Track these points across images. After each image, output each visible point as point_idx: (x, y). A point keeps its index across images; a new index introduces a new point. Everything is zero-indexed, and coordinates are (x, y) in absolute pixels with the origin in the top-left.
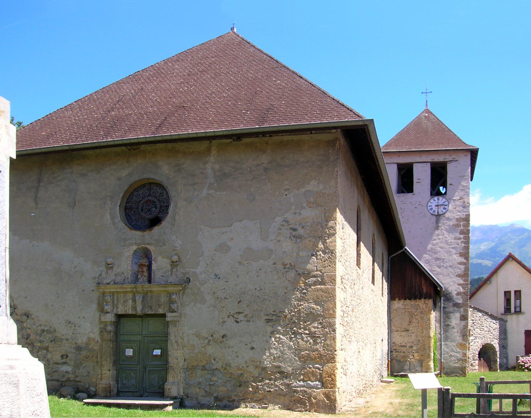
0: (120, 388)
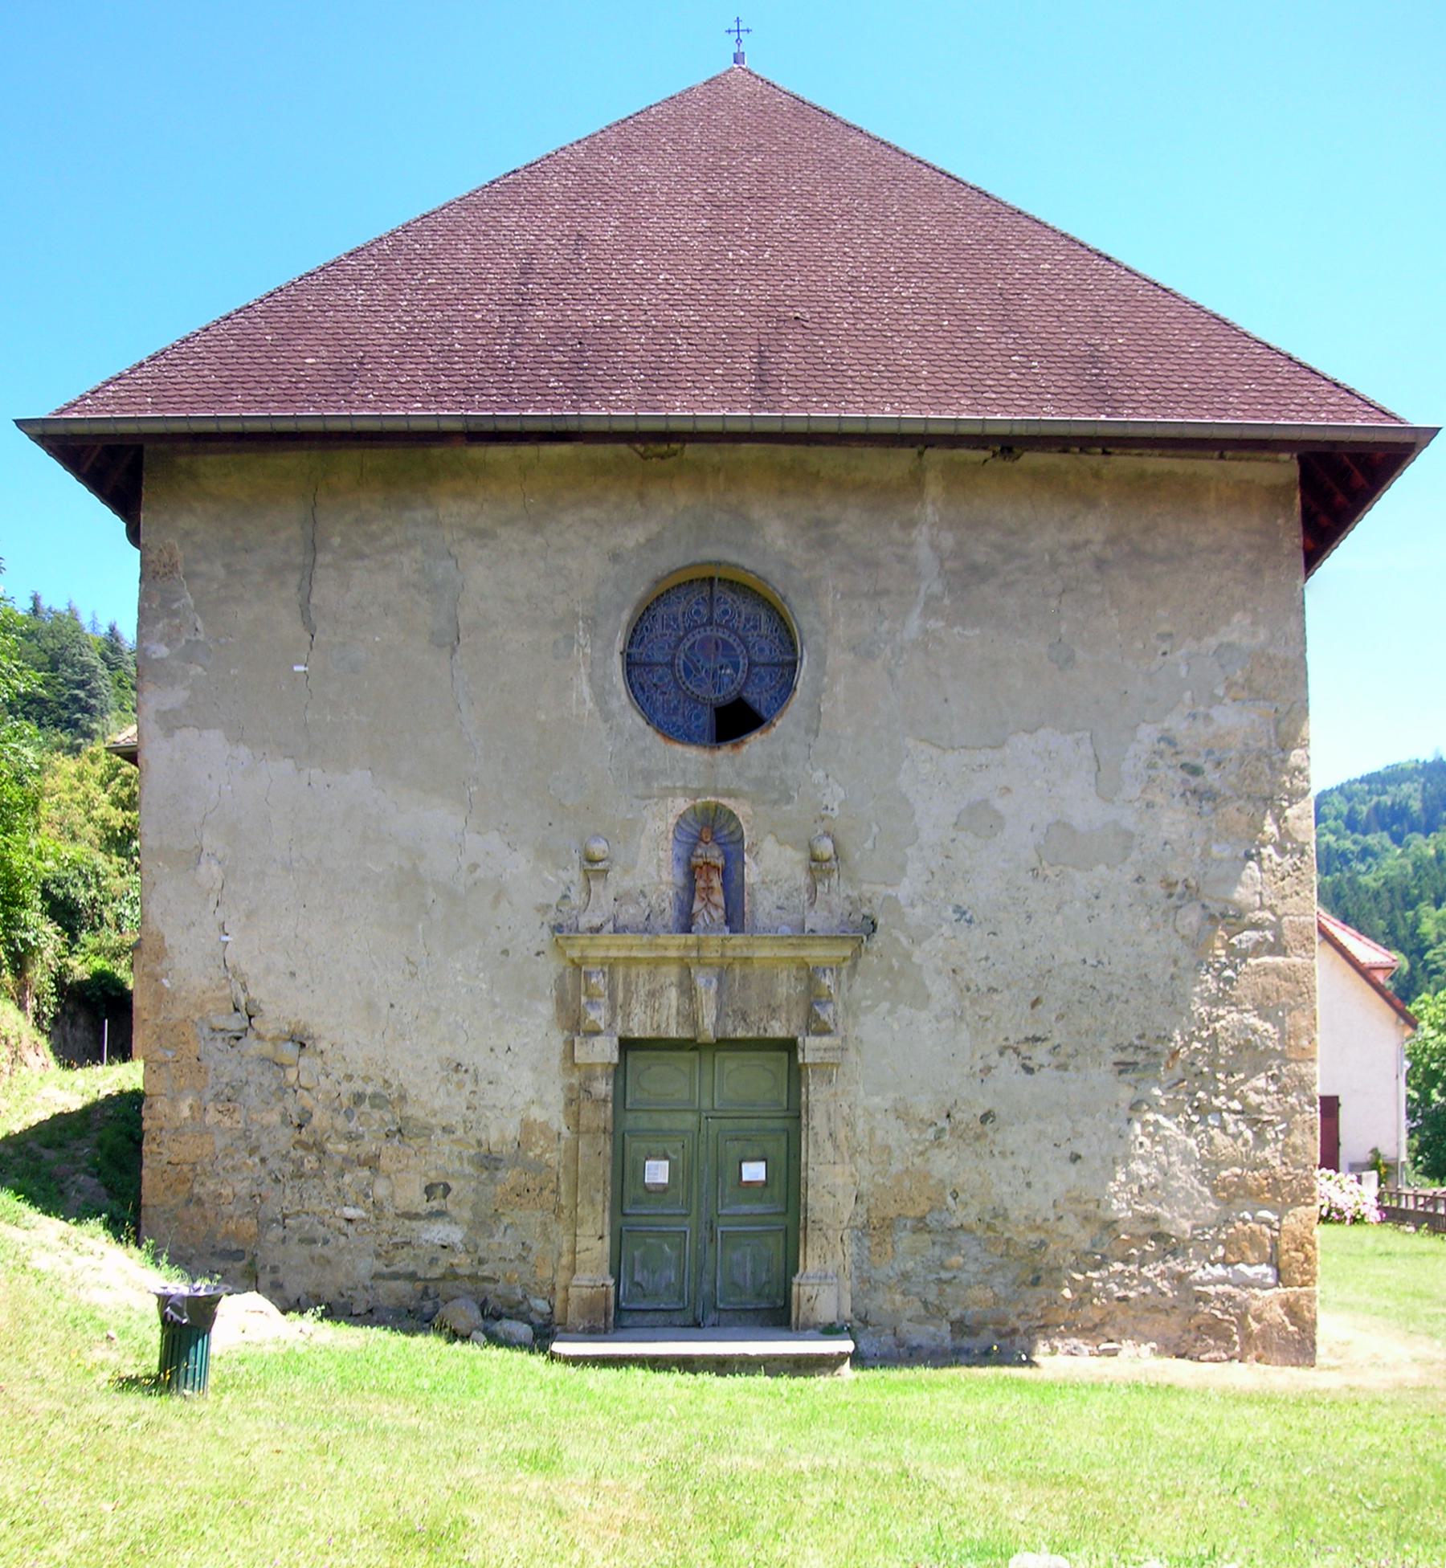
0: (624, 1300)
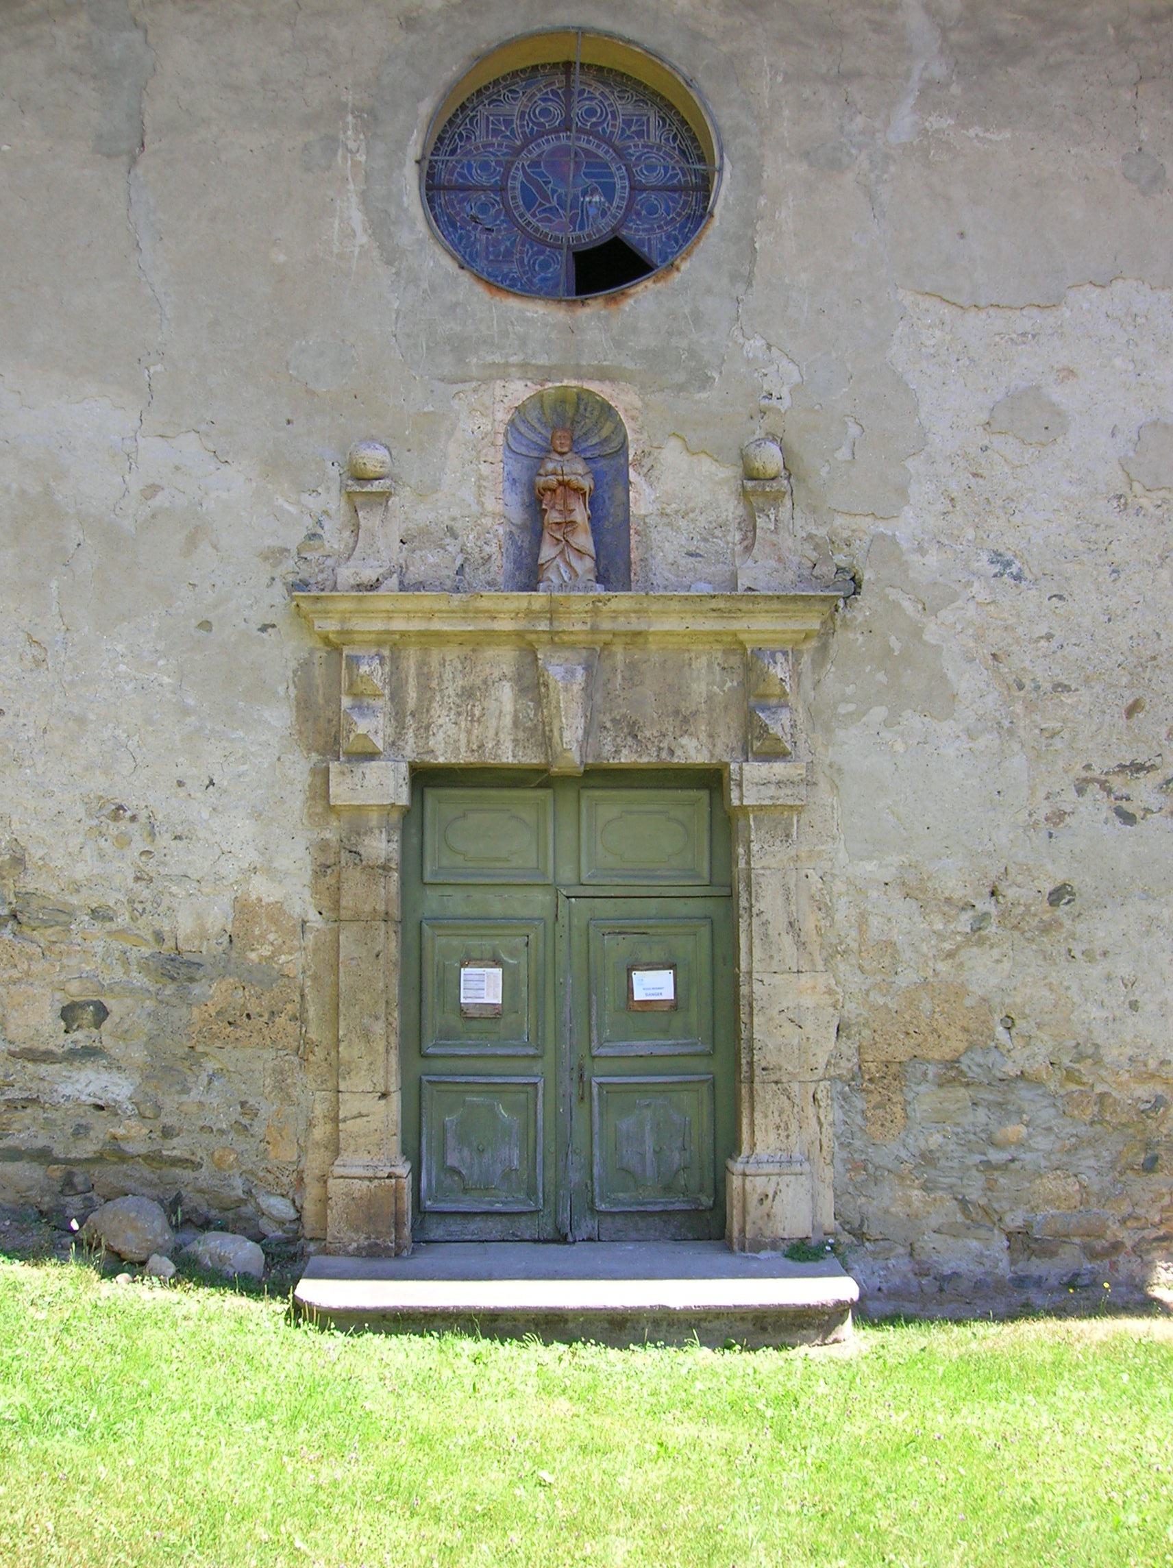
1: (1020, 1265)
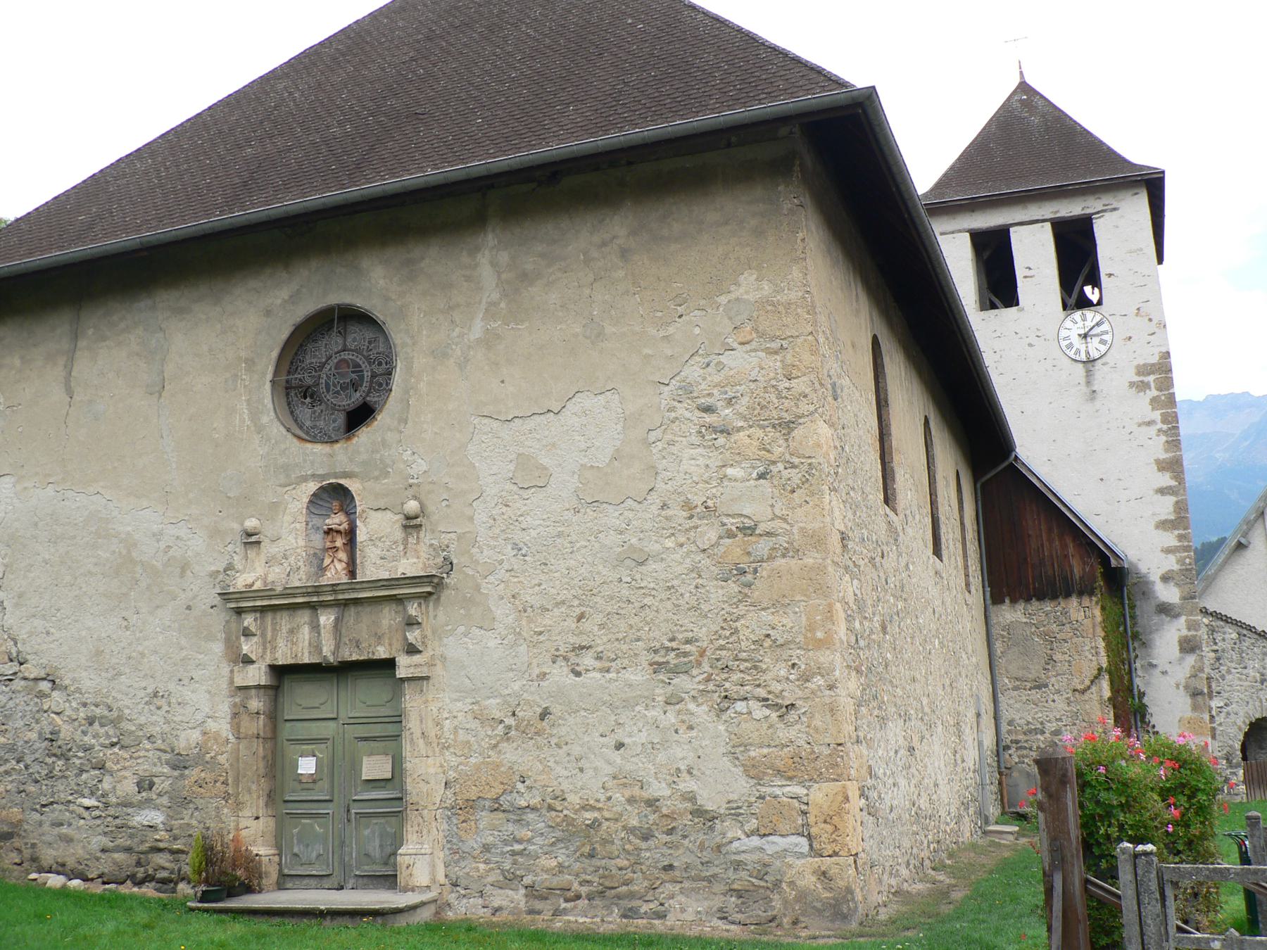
0: (286, 867)
1: (530, 903)
